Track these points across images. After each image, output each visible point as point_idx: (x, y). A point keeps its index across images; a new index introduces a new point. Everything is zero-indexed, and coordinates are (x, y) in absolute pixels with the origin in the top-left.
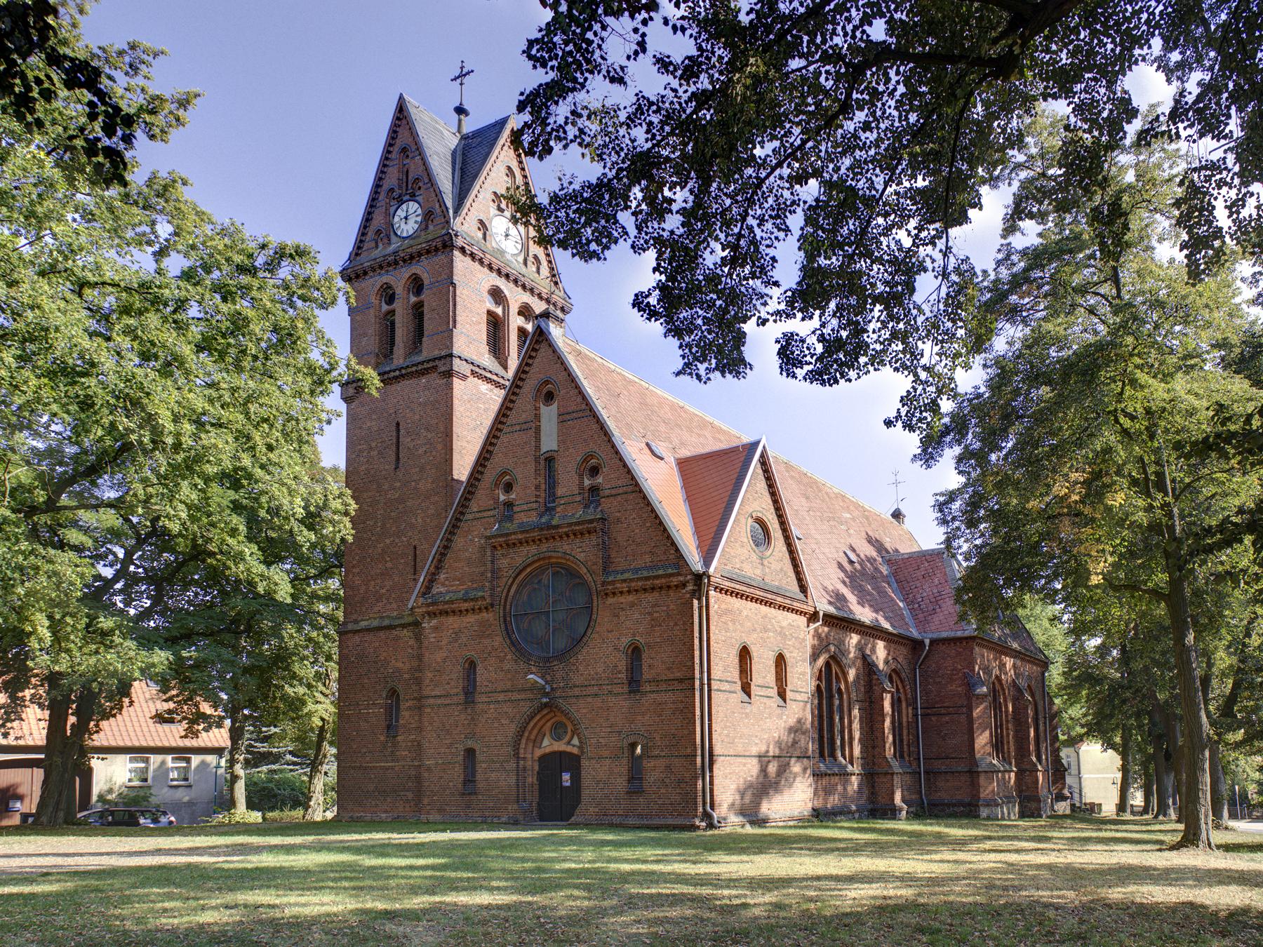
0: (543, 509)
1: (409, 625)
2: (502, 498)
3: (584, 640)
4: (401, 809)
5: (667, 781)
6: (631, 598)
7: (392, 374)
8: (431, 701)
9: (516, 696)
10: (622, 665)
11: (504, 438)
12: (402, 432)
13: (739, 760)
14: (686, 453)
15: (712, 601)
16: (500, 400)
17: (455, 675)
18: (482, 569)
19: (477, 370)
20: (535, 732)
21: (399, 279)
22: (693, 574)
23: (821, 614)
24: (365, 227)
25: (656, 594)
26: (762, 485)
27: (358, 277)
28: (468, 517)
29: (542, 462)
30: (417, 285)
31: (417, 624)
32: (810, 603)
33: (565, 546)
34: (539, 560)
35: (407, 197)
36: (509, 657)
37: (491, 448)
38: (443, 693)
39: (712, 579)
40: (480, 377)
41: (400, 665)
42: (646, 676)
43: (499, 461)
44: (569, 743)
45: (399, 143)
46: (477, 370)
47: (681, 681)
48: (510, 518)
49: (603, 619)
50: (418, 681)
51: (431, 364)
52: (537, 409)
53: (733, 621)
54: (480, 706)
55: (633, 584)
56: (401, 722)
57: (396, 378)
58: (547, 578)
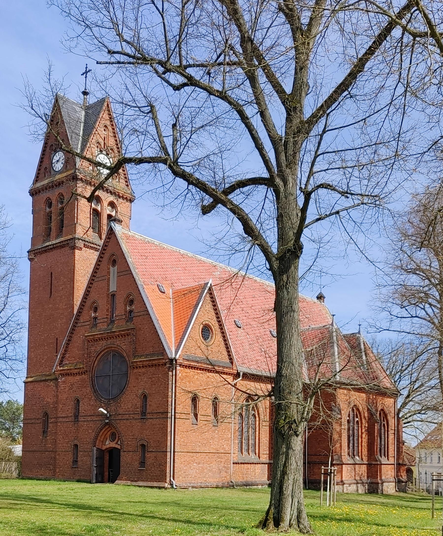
0: (109, 322)
1: (54, 379)
2: (93, 315)
3: (124, 391)
4: (48, 474)
5: (155, 464)
6: (143, 370)
7: (50, 247)
8: (61, 419)
9: (95, 418)
10: (139, 404)
11: (95, 284)
12: (53, 277)
13: (189, 454)
14: (179, 286)
15: (178, 372)
16: (96, 257)
17: (71, 405)
18: (84, 352)
19: (87, 243)
20: (103, 437)
21: (53, 195)
22: (169, 359)
23: (241, 374)
24: (40, 166)
25: (154, 368)
26: (209, 306)
27: (36, 193)
28: (79, 325)
29: (110, 297)
30: (61, 197)
31: (56, 379)
32: (235, 368)
33: (118, 342)
34: (107, 348)
35: (59, 149)
36: (93, 398)
37: (89, 290)
38: (66, 416)
39: (178, 361)
40: (88, 247)
41: (49, 400)
42: (148, 411)
43: (93, 296)
44: (117, 443)
45: (44, 166)
46: (87, 243)
47: (162, 413)
48: (95, 325)
49: (132, 380)
50: (56, 409)
51: (66, 242)
52: (109, 269)
53: (189, 382)
54: (80, 422)
55: (144, 363)
56: (49, 429)
57: (51, 249)
58: (110, 358)
